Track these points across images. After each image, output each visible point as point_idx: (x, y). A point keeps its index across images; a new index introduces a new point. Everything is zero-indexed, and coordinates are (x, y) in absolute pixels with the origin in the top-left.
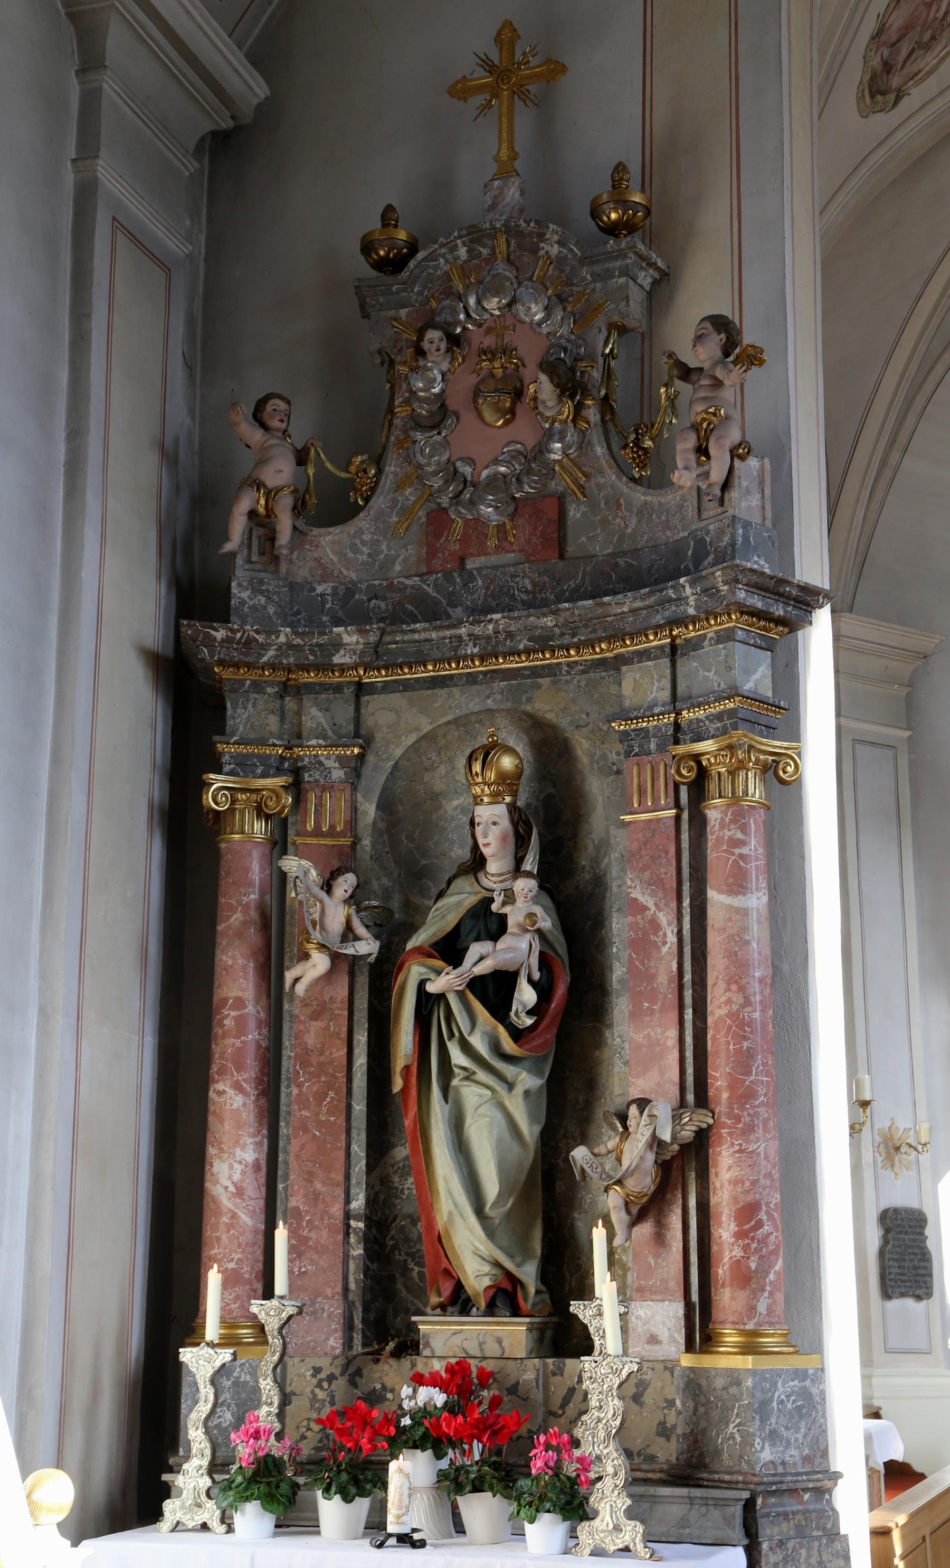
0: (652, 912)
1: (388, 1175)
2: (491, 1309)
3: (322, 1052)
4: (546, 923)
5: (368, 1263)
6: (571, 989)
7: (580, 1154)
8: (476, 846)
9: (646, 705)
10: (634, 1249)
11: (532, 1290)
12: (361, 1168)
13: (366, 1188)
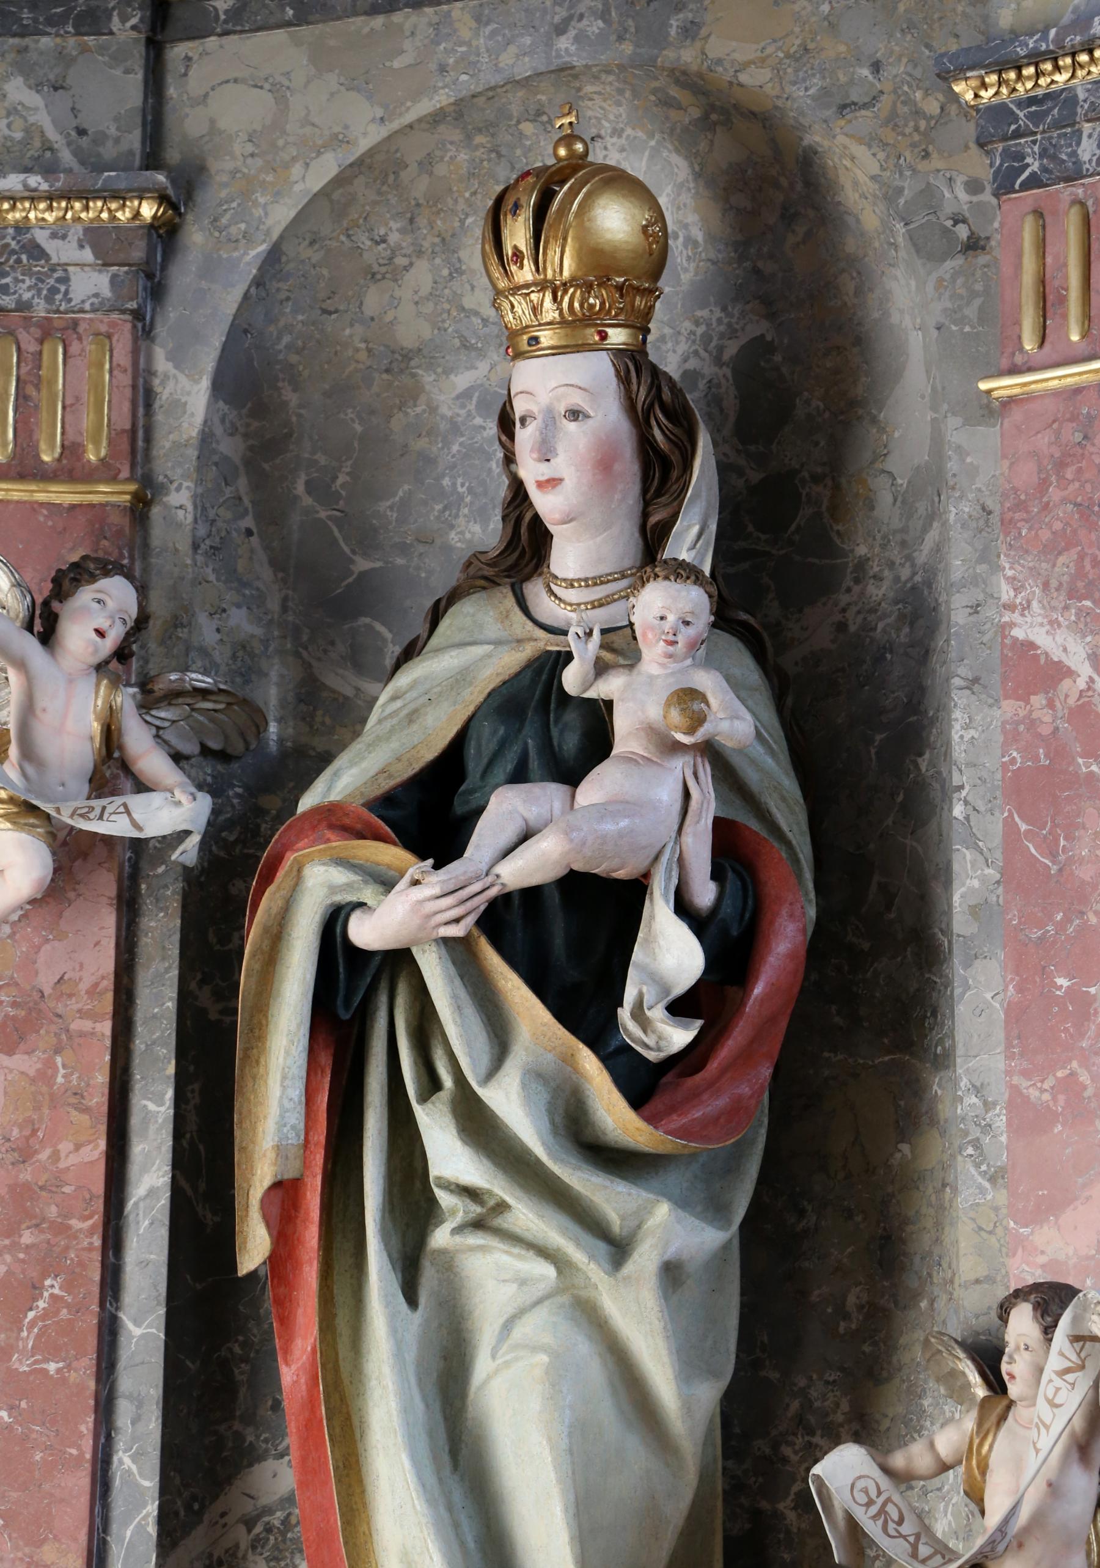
0: (1081, 683)
4: (736, 719)
8: (518, 494)
9: (1066, 19)
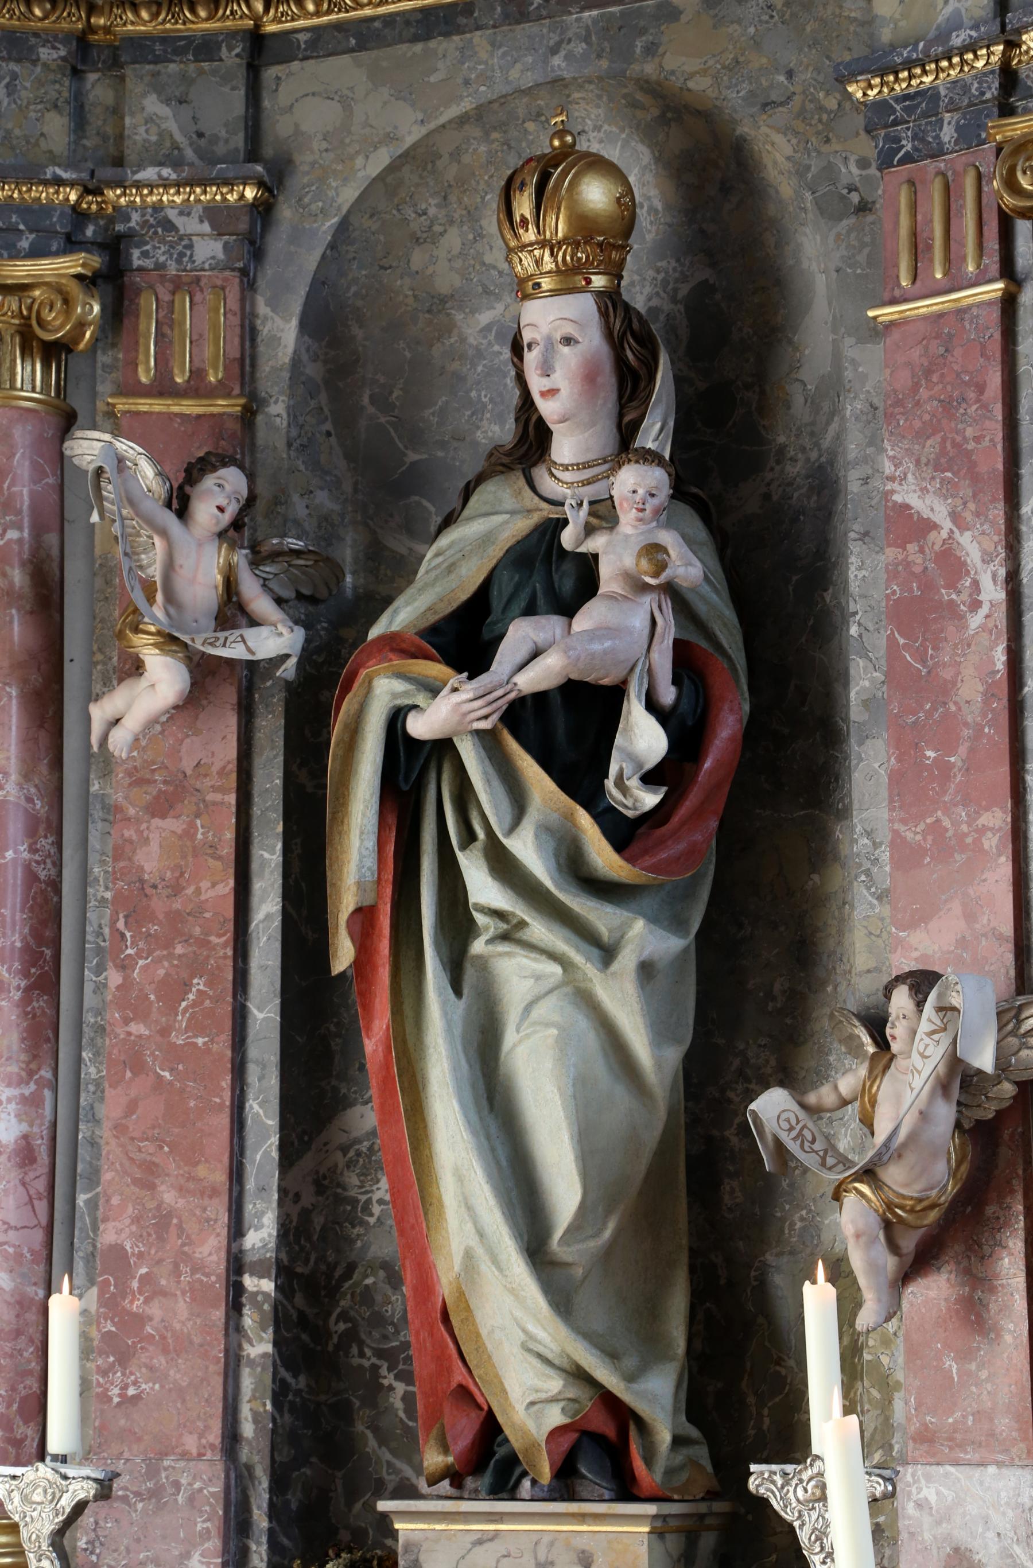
0: (944, 534)
1: (333, 1169)
2: (565, 1484)
3: (176, 889)
4: (688, 566)
5: (283, 1373)
6: (753, 732)
7: (771, 1107)
8: (527, 403)
9: (932, 34)
10: (907, 1338)
11: (664, 1437)
12: (267, 1153)
13: (281, 1202)
